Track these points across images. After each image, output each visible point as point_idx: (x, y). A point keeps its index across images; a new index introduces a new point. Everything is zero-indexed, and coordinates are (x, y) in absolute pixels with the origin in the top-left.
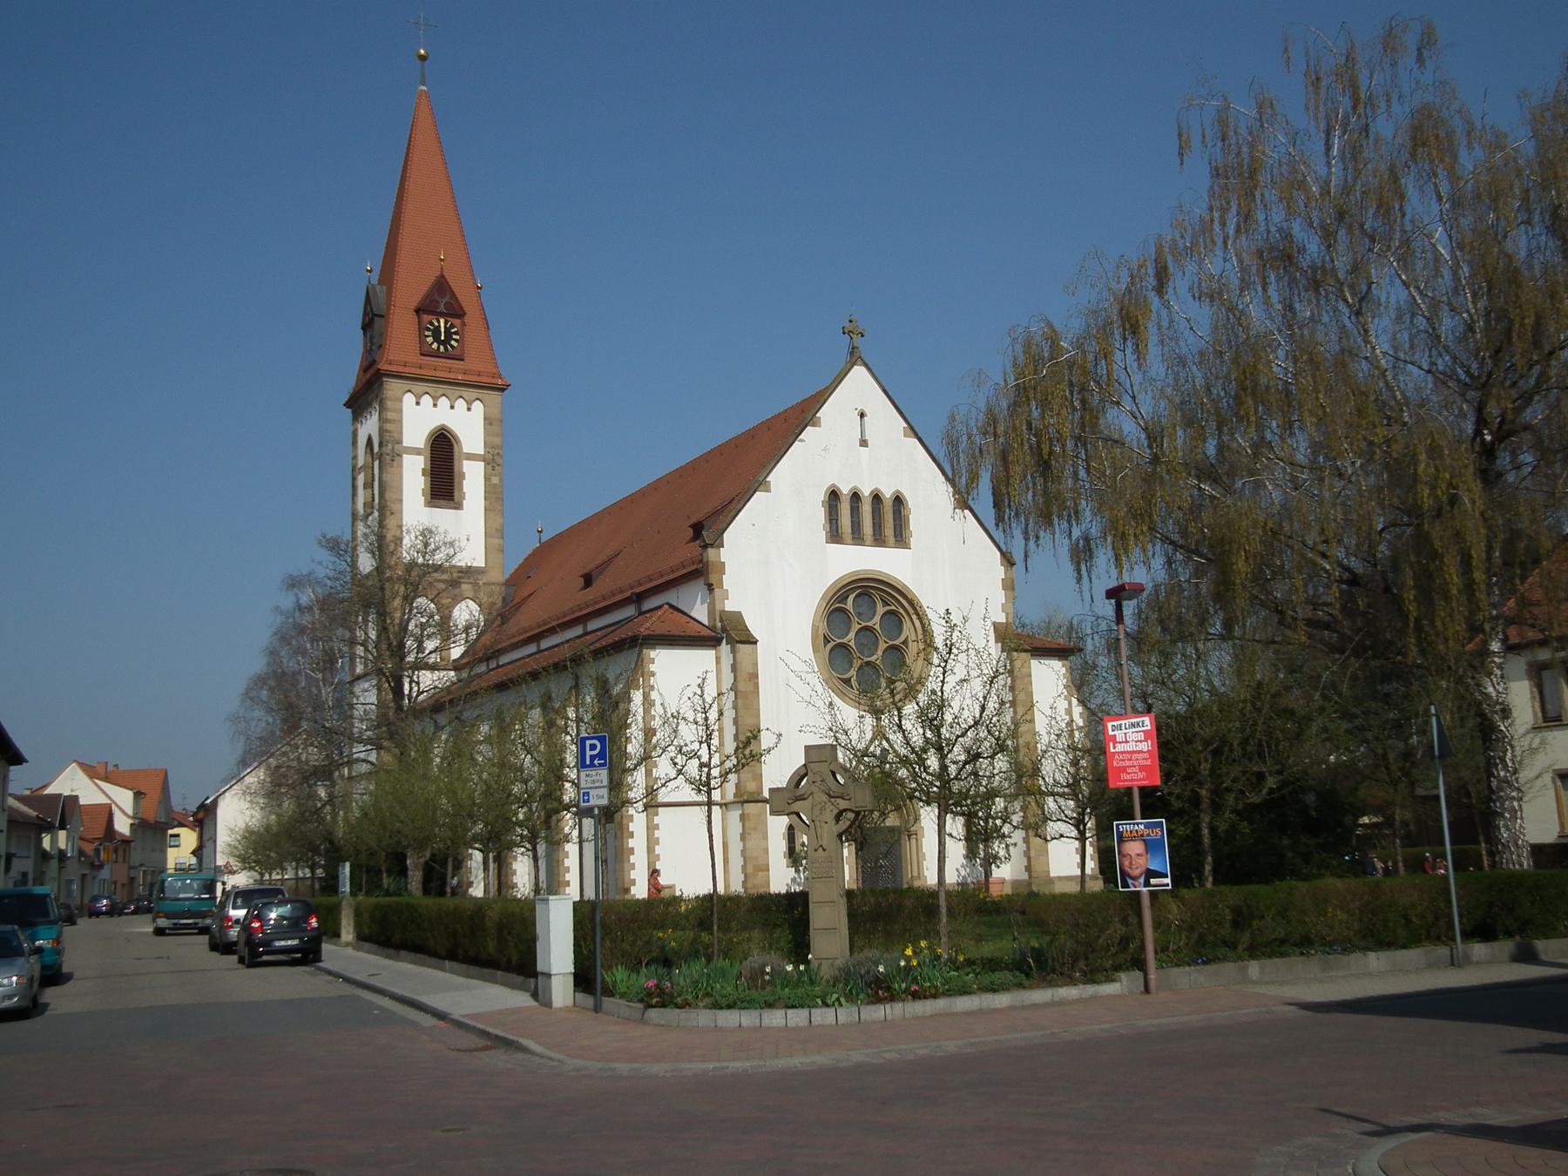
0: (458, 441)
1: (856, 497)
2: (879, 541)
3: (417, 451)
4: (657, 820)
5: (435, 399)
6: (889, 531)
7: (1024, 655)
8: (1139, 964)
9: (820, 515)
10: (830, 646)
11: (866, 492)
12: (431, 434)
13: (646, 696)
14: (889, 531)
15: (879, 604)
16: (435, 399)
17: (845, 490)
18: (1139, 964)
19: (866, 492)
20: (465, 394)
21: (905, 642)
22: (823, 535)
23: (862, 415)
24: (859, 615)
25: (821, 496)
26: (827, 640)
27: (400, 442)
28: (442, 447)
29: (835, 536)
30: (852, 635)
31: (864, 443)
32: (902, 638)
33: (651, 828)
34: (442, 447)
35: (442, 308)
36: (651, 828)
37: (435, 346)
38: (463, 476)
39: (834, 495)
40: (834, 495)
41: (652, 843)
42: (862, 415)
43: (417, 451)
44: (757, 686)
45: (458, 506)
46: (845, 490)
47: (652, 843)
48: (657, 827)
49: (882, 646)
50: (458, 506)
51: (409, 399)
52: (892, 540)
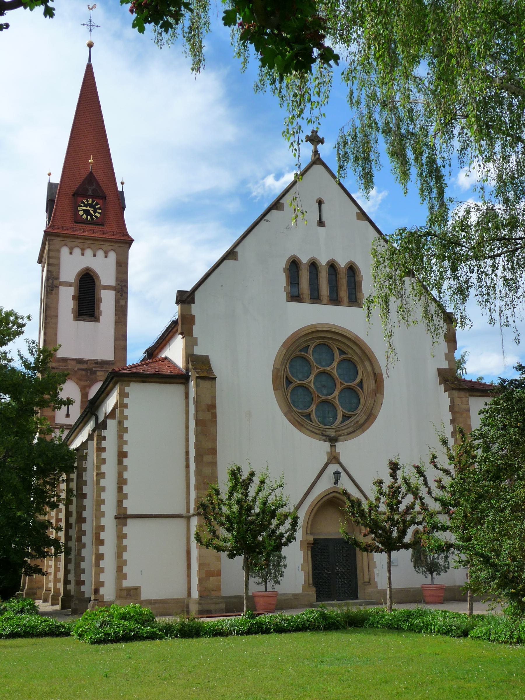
0: (98, 277)
1: (314, 265)
2: (335, 301)
3: (70, 284)
4: (125, 530)
5: (83, 250)
6: (343, 293)
7: (462, 394)
8: (248, 598)
9: (282, 279)
10: (292, 386)
11: (323, 261)
12: (371, 417)
13: (120, 423)
14: (343, 293)
15: (337, 353)
16: (83, 250)
17: (304, 259)
18: (248, 598)
19: (323, 261)
20: (103, 247)
21: (361, 384)
22: (284, 295)
23: (320, 203)
24: (319, 362)
25: (282, 264)
26: (289, 382)
27: (58, 278)
28: (87, 283)
29: (295, 297)
30: (312, 378)
31: (321, 223)
32: (358, 380)
33: (121, 536)
34: (87, 283)
35: (90, 193)
36: (121, 536)
37: (84, 216)
38: (100, 300)
39: (294, 265)
40: (294, 265)
41: (121, 549)
42: (320, 203)
43: (70, 284)
44: (214, 416)
45: (97, 320)
46: (304, 259)
47: (121, 549)
48: (125, 536)
49: (339, 387)
50: (97, 320)
51: (65, 251)
52: (346, 300)
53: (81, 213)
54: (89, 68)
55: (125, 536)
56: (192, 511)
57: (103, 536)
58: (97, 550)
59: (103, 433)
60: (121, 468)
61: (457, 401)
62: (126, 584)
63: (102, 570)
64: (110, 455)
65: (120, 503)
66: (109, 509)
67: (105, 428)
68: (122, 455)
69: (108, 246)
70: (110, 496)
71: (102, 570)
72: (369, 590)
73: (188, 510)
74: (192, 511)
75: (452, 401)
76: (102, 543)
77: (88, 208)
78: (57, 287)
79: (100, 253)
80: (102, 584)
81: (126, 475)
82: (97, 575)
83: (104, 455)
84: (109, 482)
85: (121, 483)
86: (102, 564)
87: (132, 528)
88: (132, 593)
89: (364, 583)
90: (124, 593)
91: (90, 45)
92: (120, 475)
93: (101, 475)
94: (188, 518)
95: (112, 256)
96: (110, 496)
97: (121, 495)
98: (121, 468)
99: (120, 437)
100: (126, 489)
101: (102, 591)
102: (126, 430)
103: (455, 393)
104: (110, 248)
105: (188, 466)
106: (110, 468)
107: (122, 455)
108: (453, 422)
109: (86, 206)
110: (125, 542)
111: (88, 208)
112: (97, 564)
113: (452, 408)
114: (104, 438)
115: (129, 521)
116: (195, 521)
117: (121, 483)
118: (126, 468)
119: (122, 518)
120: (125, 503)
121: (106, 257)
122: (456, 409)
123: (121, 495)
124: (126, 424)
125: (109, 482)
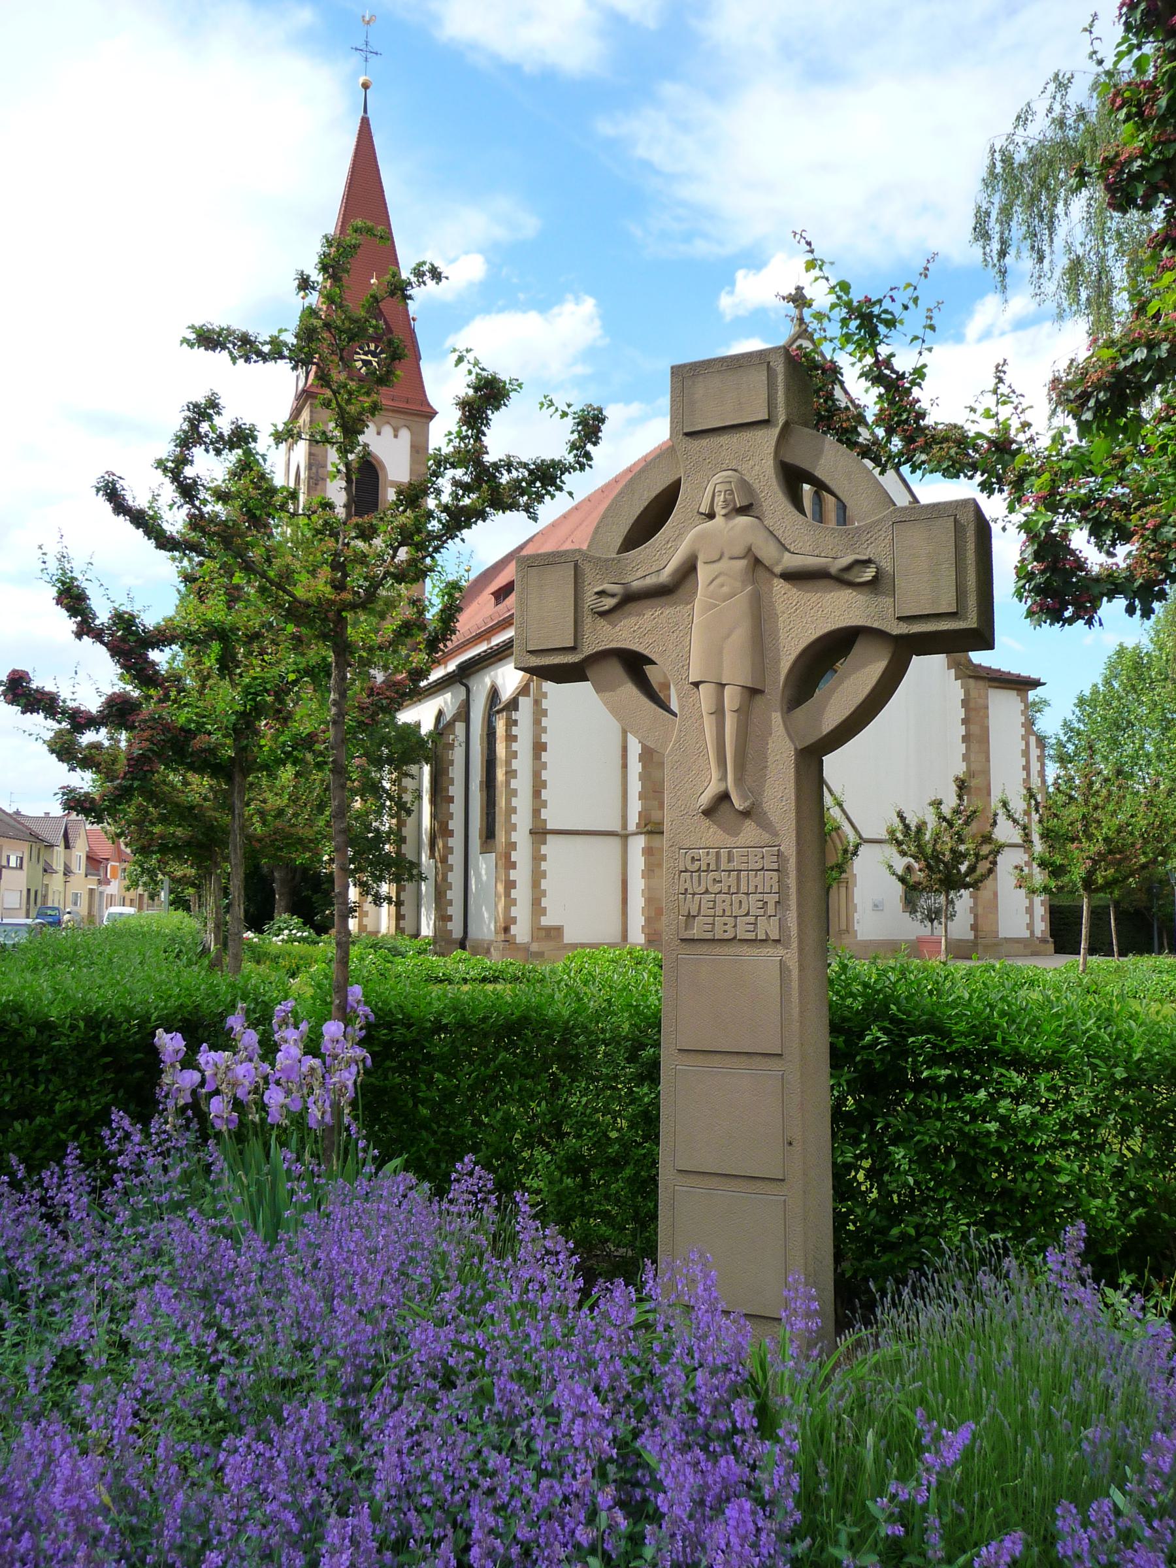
0: (383, 468)
4: (544, 850)
7: (981, 684)
13: (537, 703)
41: (537, 876)
47: (537, 876)
48: (544, 858)
53: (359, 364)
54: (365, 124)
55: (544, 858)
56: (632, 827)
57: (514, 856)
58: (507, 875)
59: (515, 715)
60: (538, 766)
61: (974, 694)
62: (545, 921)
63: (514, 902)
64: (523, 746)
65: (536, 813)
66: (523, 820)
67: (516, 709)
68: (539, 748)
69: (398, 420)
70: (523, 803)
71: (514, 902)
72: (846, 940)
73: (625, 825)
74: (632, 827)
75: (967, 693)
76: (513, 865)
77: (369, 358)
78: (324, 479)
79: (387, 431)
80: (514, 921)
81: (545, 775)
82: (507, 909)
83: (515, 746)
84: (523, 784)
85: (538, 786)
86: (514, 894)
87: (552, 847)
88: (554, 933)
89: (840, 932)
90: (543, 933)
91: (366, 86)
92: (537, 775)
93: (511, 774)
94: (624, 837)
95: (405, 434)
96: (523, 803)
97: (538, 804)
98: (538, 766)
99: (537, 722)
100: (545, 794)
101: (514, 930)
102: (545, 713)
103: (971, 681)
104: (402, 422)
105: (625, 766)
106: (523, 764)
107: (539, 748)
108: (965, 721)
109: (366, 354)
110: (544, 866)
111: (369, 358)
112: (507, 894)
113: (965, 703)
114: (515, 723)
115: (549, 837)
116: (638, 844)
117: (538, 786)
118: (544, 766)
119: (540, 833)
120: (544, 814)
121: (396, 436)
122: (972, 705)
123: (538, 804)
124: (545, 704)
125: (523, 784)
